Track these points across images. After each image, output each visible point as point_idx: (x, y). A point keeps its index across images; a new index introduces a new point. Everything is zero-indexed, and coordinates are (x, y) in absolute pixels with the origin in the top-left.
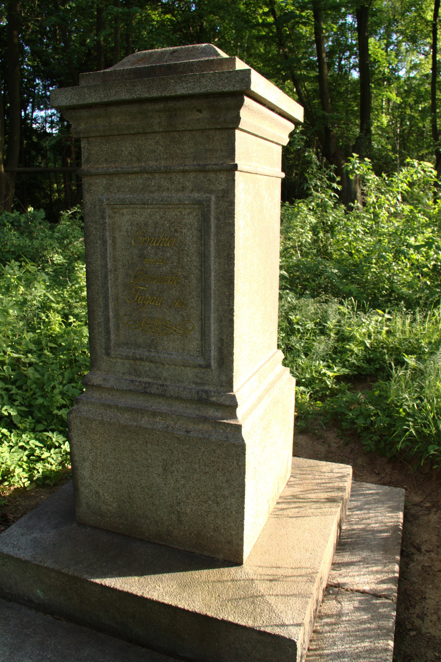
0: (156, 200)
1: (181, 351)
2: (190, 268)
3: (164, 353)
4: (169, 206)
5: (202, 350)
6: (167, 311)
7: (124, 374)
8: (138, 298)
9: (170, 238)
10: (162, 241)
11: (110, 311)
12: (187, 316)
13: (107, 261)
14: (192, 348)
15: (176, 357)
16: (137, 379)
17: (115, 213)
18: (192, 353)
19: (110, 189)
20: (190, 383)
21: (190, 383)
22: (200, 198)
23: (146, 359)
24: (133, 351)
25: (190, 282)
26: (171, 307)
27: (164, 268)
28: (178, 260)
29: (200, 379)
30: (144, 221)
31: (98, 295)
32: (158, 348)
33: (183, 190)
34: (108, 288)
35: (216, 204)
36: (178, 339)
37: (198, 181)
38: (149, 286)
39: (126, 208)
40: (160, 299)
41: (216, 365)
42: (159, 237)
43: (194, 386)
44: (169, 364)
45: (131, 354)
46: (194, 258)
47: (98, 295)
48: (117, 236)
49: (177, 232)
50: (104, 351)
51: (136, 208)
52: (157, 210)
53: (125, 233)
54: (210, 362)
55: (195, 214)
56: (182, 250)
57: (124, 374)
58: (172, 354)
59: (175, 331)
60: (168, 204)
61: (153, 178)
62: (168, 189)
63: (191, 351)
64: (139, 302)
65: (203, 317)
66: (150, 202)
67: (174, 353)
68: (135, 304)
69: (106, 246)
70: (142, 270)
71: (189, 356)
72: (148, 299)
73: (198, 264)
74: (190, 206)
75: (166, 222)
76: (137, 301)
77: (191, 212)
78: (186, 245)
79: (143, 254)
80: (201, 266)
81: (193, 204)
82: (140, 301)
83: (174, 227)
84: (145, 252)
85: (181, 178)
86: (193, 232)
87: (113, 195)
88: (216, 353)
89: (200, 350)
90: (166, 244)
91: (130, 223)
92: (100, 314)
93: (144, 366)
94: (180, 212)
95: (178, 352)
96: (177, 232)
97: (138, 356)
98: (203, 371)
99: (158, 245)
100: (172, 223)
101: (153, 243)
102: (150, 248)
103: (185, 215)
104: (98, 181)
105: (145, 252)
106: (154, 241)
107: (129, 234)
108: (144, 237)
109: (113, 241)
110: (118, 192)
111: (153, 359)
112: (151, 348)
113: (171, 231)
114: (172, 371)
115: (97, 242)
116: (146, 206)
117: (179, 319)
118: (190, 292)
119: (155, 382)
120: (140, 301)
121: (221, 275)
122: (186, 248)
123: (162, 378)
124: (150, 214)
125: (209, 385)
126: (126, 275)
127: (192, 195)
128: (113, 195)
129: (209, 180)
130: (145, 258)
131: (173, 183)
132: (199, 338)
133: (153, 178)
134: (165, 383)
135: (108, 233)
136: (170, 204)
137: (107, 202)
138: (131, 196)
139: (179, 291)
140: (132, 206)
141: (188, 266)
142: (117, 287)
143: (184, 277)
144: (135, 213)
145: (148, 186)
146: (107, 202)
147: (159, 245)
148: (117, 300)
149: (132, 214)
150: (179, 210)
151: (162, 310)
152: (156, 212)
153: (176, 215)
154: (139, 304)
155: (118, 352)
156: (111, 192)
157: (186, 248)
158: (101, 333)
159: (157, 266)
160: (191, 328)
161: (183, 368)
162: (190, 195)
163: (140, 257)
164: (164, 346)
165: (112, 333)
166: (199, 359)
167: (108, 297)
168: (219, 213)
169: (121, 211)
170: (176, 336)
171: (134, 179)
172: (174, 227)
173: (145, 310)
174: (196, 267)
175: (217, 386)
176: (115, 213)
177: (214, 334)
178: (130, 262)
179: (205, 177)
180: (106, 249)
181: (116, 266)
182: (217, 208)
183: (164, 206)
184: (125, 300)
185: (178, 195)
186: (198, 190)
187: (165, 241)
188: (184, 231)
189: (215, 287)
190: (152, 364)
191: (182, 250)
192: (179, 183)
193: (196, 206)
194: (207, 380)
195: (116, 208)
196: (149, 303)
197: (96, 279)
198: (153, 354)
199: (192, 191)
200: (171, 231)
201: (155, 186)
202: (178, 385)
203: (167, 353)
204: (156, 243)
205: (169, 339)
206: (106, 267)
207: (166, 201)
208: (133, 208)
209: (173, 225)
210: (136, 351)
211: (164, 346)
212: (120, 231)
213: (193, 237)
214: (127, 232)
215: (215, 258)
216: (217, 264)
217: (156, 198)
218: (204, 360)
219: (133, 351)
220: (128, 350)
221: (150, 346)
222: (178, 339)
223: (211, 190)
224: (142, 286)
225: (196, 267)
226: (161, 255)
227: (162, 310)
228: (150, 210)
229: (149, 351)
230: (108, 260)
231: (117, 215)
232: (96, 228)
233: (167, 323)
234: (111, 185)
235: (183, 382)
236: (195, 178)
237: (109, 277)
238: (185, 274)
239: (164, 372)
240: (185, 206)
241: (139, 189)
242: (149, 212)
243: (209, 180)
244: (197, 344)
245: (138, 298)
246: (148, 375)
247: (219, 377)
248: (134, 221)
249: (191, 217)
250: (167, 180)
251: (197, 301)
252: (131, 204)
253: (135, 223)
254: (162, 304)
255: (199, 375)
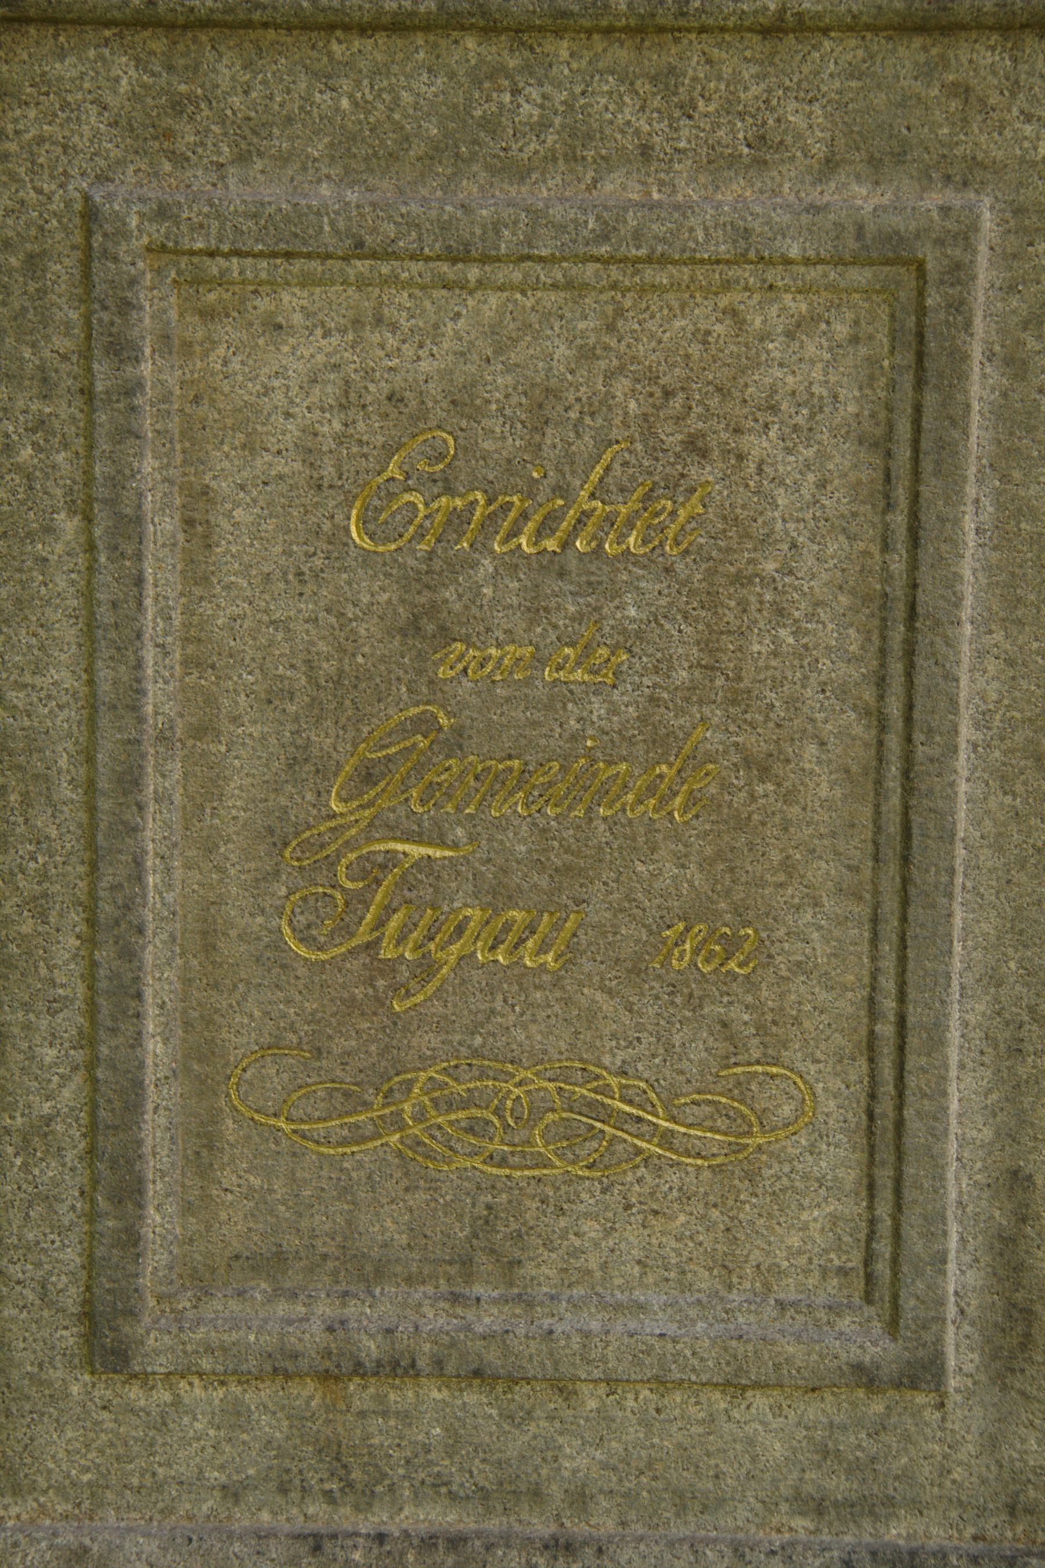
0: (562, 228)
1: (705, 1281)
2: (793, 703)
3: (575, 1306)
4: (649, 273)
5: (868, 1260)
6: (607, 1005)
7: (232, 1493)
8: (380, 924)
9: (647, 497)
10: (584, 516)
11: (151, 1027)
12: (761, 1029)
13: (139, 665)
14: (793, 1253)
15: (672, 1329)
16: (345, 1517)
17: (208, 314)
18: (788, 1290)
19: (169, 134)
20: (770, 1506)
21: (770, 1506)
22: (896, 221)
23: (439, 1363)
24: (325, 1309)
25: (789, 798)
26: (637, 971)
27: (598, 708)
28: (707, 646)
29: (853, 1469)
30: (446, 374)
31: (43, 916)
32: (529, 1269)
33: (761, 163)
34: (138, 862)
35: (1006, 258)
36: (686, 1197)
37: (880, 99)
38: (472, 838)
39: (307, 281)
40: (557, 927)
41: (972, 1360)
42: (561, 490)
43: (801, 1523)
44: (611, 1382)
45: (315, 1335)
46: (829, 633)
47: (43, 916)
48: (224, 486)
49: (704, 454)
50: (69, 1338)
51: (392, 280)
52: (553, 297)
53: (291, 466)
54: (939, 1340)
55: (841, 330)
56: (739, 579)
57: (232, 1493)
58: (641, 1307)
59: (666, 1139)
60: (649, 260)
61: (527, 68)
62: (646, 151)
63: (781, 1273)
64: (387, 952)
65: (886, 1029)
66: (507, 242)
67: (656, 1300)
68: (355, 965)
69: (139, 556)
70: (424, 724)
71: (770, 1311)
72: (460, 930)
73: (855, 673)
74: (814, 273)
75: (621, 386)
76: (372, 946)
77: (815, 319)
78: (765, 541)
79: (433, 610)
80: (881, 682)
81: (839, 262)
82: (401, 939)
83: (679, 419)
84: (449, 594)
85: (748, 72)
86: (823, 456)
87: (200, 178)
88: (972, 1278)
89: (855, 1260)
90: (621, 539)
91: (331, 392)
92: (50, 1054)
93: (404, 1416)
94: (732, 312)
95: (687, 1287)
96: (704, 454)
97: (371, 1347)
98: (877, 1407)
99: (551, 544)
100: (668, 394)
101: (514, 533)
102: (487, 565)
103: (764, 337)
104: (66, 69)
105: (449, 594)
106: (525, 516)
107: (328, 471)
108: (449, 490)
109: (189, 523)
110: (243, 158)
111: (492, 1356)
112: (469, 1278)
113: (655, 451)
114: (634, 1433)
115: (49, 530)
116: (474, 273)
117: (697, 1052)
118: (788, 866)
119: (494, 1524)
120: (401, 939)
121: (1019, 737)
122: (770, 567)
123: (555, 1490)
124: (494, 329)
125: (918, 1508)
126: (292, 764)
127: (828, 194)
128: (200, 178)
129: (962, 91)
130: (445, 636)
131: (688, 110)
132: (850, 1177)
133: (527, 68)
134: (576, 1527)
135: (149, 464)
136: (664, 261)
137: (157, 231)
138: (352, 196)
139: (706, 864)
140: (361, 266)
141: (776, 685)
142: (210, 850)
143: (748, 762)
144: (379, 320)
145: (490, 125)
146: (157, 231)
147: (566, 544)
148: (209, 948)
149: (357, 323)
150: (724, 301)
151: (567, 1002)
152: (547, 316)
153: (704, 337)
154: (390, 967)
155: (200, 1333)
156: (179, 160)
157: (770, 567)
158: (49, 1200)
159: (540, 692)
160: (787, 1110)
161: (720, 1402)
162: (814, 195)
163: (413, 627)
164: (575, 1253)
165: (154, 1189)
166: (846, 1323)
167: (140, 930)
168: (1025, 325)
169: (264, 304)
170: (673, 1177)
171: (376, 72)
172: (679, 419)
173: (438, 1007)
174: (843, 692)
175: (982, 1511)
176: (208, 314)
177: (963, 1142)
178: (329, 667)
179: (926, 72)
180: (139, 581)
181: (210, 701)
182: (1011, 288)
183: (615, 272)
184: (278, 944)
185: (726, 196)
186: (874, 162)
187: (610, 520)
188: (756, 446)
189: (978, 823)
190: (471, 1398)
191: (739, 579)
192: (730, 107)
193: (859, 276)
194: (905, 1476)
195: (222, 281)
196: (466, 958)
197: (26, 800)
198: (488, 1320)
199: (830, 164)
200: (655, 451)
201: (542, 126)
202: (679, 1530)
203: (603, 1305)
204: (539, 534)
205: (615, 1197)
206: (135, 708)
207: (637, 236)
208: (362, 283)
209: (677, 403)
210: (351, 1310)
211: (575, 1253)
212: (251, 447)
213: (822, 484)
214: (309, 454)
215: (983, 625)
216: (992, 666)
217: (557, 212)
218: (893, 1326)
219: (325, 1309)
220: (282, 1308)
221: (466, 1263)
222: (686, 1197)
223: (974, 163)
224: (417, 838)
225: (843, 692)
226: (578, 618)
227: (567, 1002)
228: (494, 300)
229: (455, 1298)
230: (150, 655)
231: (227, 331)
232: (41, 424)
233: (605, 1090)
234: (177, 106)
235: (718, 1503)
236: (853, 73)
237: (151, 783)
238: (757, 744)
239: (569, 1445)
240: (772, 275)
241: (418, 148)
242: (488, 313)
243: (962, 91)
244: (834, 1219)
245: (380, 924)
246: (440, 1482)
247: (992, 1443)
248: (368, 374)
249: (811, 350)
250: (643, 87)
251: (841, 921)
252: (359, 249)
253: (377, 390)
254: (570, 956)
255: (846, 1442)
